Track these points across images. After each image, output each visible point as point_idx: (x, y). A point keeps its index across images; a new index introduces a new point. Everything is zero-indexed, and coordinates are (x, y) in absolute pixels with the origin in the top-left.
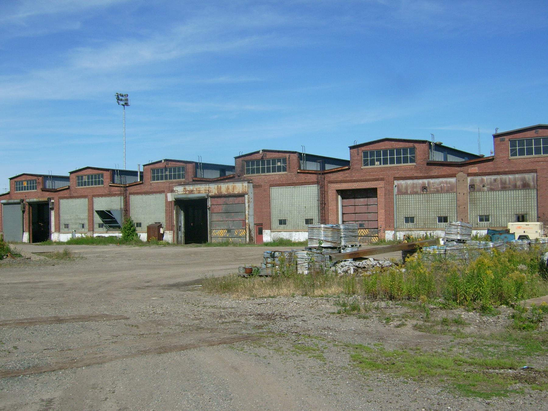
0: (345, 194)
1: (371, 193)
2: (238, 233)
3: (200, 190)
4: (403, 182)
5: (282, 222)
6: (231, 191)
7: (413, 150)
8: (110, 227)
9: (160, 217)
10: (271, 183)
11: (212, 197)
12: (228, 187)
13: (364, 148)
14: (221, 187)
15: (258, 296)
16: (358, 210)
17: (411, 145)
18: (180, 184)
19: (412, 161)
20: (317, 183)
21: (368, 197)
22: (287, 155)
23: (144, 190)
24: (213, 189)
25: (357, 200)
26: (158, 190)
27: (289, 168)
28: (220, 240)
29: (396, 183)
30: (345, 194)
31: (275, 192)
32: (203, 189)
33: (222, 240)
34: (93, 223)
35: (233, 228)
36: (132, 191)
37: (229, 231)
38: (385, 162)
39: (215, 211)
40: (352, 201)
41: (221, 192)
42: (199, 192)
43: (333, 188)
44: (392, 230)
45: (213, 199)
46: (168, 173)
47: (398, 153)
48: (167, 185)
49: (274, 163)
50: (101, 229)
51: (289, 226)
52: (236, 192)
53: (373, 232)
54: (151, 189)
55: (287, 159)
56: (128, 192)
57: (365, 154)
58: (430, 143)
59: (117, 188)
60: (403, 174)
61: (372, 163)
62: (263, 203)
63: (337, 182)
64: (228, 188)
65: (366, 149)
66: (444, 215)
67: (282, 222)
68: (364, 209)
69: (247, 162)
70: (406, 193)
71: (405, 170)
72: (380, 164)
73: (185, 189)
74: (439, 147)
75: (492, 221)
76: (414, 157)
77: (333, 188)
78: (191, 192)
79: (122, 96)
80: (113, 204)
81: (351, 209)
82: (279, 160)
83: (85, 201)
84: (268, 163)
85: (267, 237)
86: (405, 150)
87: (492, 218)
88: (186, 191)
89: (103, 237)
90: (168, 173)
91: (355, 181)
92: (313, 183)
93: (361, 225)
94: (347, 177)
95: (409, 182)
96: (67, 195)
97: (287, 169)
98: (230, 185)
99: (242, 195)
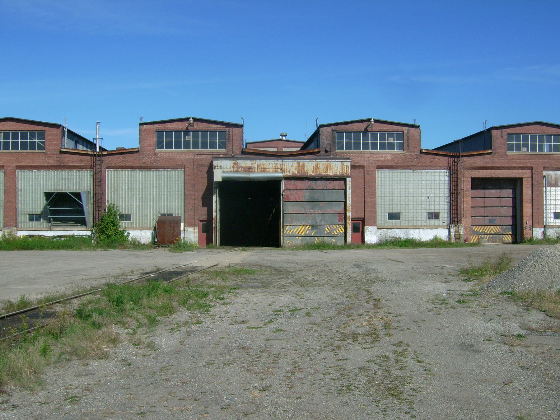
0: (478, 184)
2: (331, 231)
3: (267, 169)
5: (393, 216)
7: (42, 135)
8: (55, 219)
9: (176, 206)
10: (379, 164)
11: (287, 179)
12: (317, 165)
13: (509, 130)
14: (304, 165)
15: (41, 314)
16: (488, 202)
18: (226, 157)
20: (92, 167)
21: (500, 188)
22: (405, 129)
23: (141, 163)
24: (291, 167)
25: (487, 191)
26: (170, 164)
27: (408, 146)
28: (298, 241)
29: (545, 173)
30: (478, 184)
31: (383, 178)
32: (271, 166)
33: (302, 240)
34: (16, 212)
35: (323, 223)
36: (113, 163)
37: (314, 226)
41: (305, 173)
42: (264, 170)
43: (466, 176)
44: (541, 227)
45: (289, 182)
46: (190, 139)
47: (24, 136)
48: (191, 156)
49: (383, 138)
50: (35, 223)
51: (402, 221)
52: (331, 173)
53: (505, 229)
54: (155, 161)
55: (405, 135)
56: (104, 165)
57: (510, 137)
58: (63, 127)
59: (77, 156)
61: (518, 148)
62: (367, 189)
63: (473, 168)
64: (317, 168)
65: (512, 132)
66: (396, 212)
67: (393, 216)
68: (496, 202)
69: (340, 132)
72: (528, 150)
73: (235, 164)
74: (72, 135)
75: (133, 220)
76: (44, 143)
77: (466, 176)
78: (249, 169)
80: (78, 181)
81: (480, 202)
82: (391, 134)
84: (374, 137)
85: (371, 236)
86: (33, 134)
87: (134, 218)
88: (238, 168)
89: (73, 236)
90: (190, 139)
91: (509, 169)
92: (441, 168)
93: (491, 221)
94: (487, 163)
97: (405, 147)
99: (343, 178)
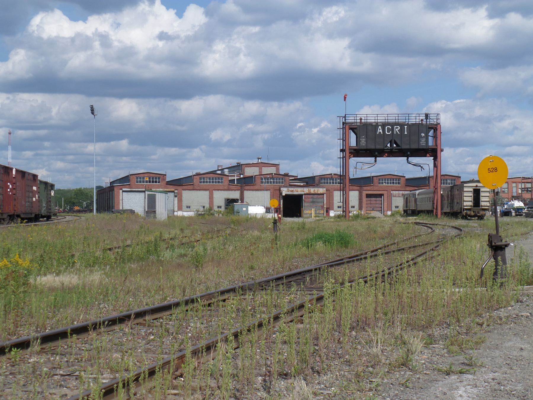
0: (368, 196)
1: (381, 196)
3: (298, 191)
4: (394, 192)
6: (316, 192)
17: (158, 176)
19: (399, 183)
24: (306, 190)
38: (388, 183)
39: (306, 201)
40: (369, 199)
43: (364, 193)
57: (379, 180)
60: (398, 189)
69: (322, 178)
70: (396, 196)
71: (396, 187)
77: (364, 193)
79: (435, 137)
81: (369, 202)
83: (207, 193)
86: (396, 179)
91: (370, 190)
95: (397, 192)
96: (191, 188)
98: (316, 189)
99: (323, 194)
